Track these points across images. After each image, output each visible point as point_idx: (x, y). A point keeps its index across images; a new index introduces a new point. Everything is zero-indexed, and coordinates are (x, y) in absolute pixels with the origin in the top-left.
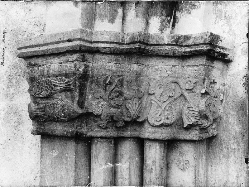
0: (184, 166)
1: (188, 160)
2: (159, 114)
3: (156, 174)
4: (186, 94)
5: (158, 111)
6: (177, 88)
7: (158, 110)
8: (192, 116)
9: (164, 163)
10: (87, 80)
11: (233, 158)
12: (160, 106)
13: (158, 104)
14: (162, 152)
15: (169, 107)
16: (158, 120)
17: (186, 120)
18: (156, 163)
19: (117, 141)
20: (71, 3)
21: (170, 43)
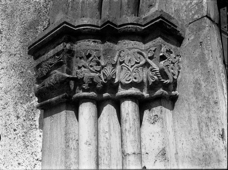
0: (154, 120)
1: (157, 114)
2: (128, 75)
3: (130, 124)
4: (149, 61)
5: (128, 73)
6: (142, 57)
7: (128, 72)
8: (155, 75)
9: (136, 115)
10: (73, 56)
11: (194, 109)
12: (129, 70)
13: (127, 68)
14: (134, 106)
15: (136, 69)
16: (128, 80)
17: (151, 79)
18: (129, 115)
19: (99, 105)
20: (147, 168)
21: (132, 22)
